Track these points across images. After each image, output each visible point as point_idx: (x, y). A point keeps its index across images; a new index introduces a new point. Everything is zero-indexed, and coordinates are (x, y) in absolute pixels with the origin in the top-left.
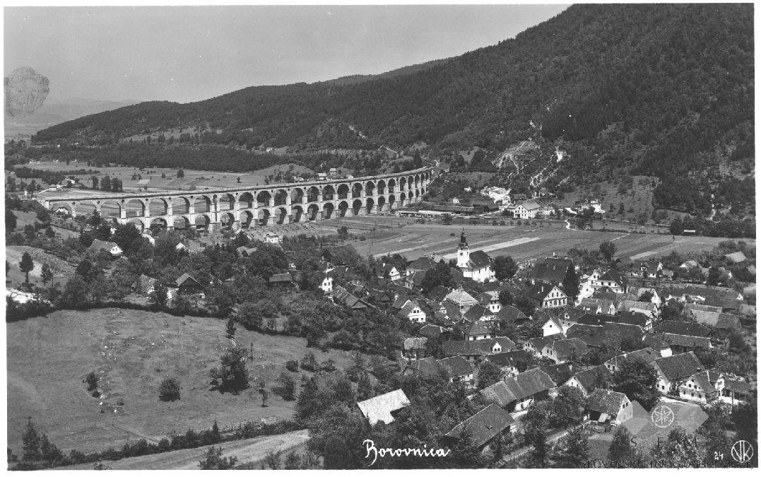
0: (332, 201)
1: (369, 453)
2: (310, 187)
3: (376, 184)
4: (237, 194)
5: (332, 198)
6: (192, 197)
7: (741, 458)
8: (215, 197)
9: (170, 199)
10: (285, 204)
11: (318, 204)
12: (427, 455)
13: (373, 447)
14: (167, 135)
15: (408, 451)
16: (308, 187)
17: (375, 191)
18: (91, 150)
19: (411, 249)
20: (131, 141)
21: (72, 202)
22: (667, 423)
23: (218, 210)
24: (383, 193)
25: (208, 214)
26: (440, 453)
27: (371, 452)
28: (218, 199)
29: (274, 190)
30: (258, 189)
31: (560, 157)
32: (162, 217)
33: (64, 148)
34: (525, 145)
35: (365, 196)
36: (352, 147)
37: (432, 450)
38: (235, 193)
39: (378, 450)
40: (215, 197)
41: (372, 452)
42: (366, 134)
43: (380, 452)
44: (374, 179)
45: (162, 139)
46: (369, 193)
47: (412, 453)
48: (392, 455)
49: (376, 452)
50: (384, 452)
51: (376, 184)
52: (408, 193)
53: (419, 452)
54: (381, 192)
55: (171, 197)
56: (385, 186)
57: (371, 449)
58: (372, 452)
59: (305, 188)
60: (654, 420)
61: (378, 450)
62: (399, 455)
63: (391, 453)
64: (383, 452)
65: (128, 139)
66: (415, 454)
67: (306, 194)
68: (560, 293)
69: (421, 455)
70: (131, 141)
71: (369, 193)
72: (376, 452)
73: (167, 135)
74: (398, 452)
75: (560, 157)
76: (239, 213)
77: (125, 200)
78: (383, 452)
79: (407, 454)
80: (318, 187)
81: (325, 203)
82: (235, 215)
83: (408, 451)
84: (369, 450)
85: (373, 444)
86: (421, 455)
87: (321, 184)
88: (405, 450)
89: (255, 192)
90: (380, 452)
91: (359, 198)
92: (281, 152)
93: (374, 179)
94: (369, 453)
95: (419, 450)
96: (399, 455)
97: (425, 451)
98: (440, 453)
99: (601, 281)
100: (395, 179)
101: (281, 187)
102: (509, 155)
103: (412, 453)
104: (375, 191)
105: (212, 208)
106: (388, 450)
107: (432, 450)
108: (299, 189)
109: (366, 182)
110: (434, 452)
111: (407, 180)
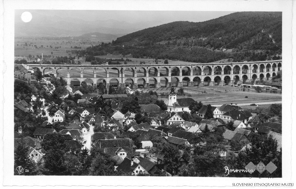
0: (189, 77)
1: (226, 171)
3: (232, 68)
4: (170, 67)
5: (230, 74)
6: (108, 68)
7: (19, 172)
8: (122, 69)
9: (108, 68)
11: (230, 76)
12: (247, 172)
13: (228, 169)
15: (240, 170)
16: (215, 66)
19: (204, 102)
22: (263, 170)
23: (124, 76)
24: (263, 71)
25: (167, 77)
26: (251, 171)
28: (123, 70)
29: (160, 67)
30: (149, 66)
32: (132, 78)
35: (272, 71)
37: (249, 170)
38: (135, 67)
39: (230, 170)
40: (122, 69)
43: (230, 171)
44: (231, 64)
46: (262, 70)
47: (242, 171)
51: (232, 68)
52: (272, 73)
55: (96, 67)
56: (264, 67)
57: (227, 170)
58: (227, 171)
59: (223, 66)
60: (258, 169)
62: (237, 172)
63: (234, 171)
66: (243, 171)
67: (192, 71)
68: (155, 123)
69: (245, 172)
71: (262, 70)
74: (237, 171)
77: (70, 67)
79: (240, 172)
80: (221, 66)
81: (184, 77)
82: (168, 79)
83: (240, 170)
86: (245, 172)
87: (192, 65)
88: (239, 170)
91: (219, 75)
93: (231, 64)
94: (226, 171)
95: (244, 170)
96: (237, 172)
98: (251, 171)
103: (242, 171)
104: (265, 70)
107: (249, 170)
108: (228, 66)
110: (249, 171)
111: (259, 67)
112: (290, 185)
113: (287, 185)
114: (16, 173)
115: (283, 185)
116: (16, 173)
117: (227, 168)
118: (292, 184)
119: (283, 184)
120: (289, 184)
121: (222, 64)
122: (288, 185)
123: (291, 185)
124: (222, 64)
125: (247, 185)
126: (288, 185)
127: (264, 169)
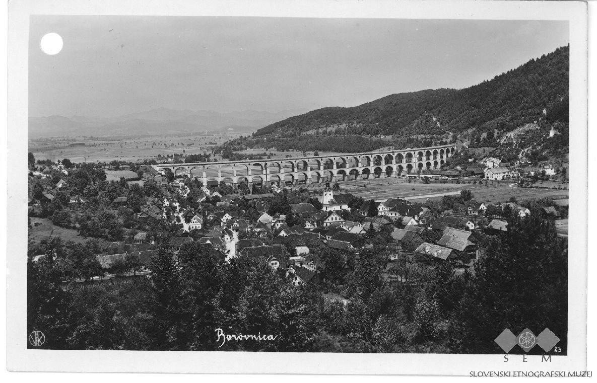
2: (386, 154)
6: (249, 164)
9: (249, 164)
10: (345, 167)
13: (222, 334)
14: (329, 130)
15: (247, 336)
17: (432, 157)
18: (283, 140)
20: (307, 134)
21: (233, 164)
22: (530, 344)
23: (268, 172)
26: (270, 338)
27: (220, 337)
29: (310, 159)
31: (552, 134)
33: (269, 141)
34: (528, 127)
36: (429, 133)
37: (265, 336)
39: (226, 336)
41: (222, 337)
42: (441, 124)
43: (227, 337)
45: (325, 133)
47: (250, 338)
48: (236, 339)
49: (224, 337)
50: (230, 337)
53: (255, 337)
54: (428, 159)
57: (221, 335)
58: (222, 337)
61: (226, 336)
63: (235, 338)
64: (229, 338)
65: (305, 133)
70: (307, 134)
72: (224, 337)
73: (329, 130)
75: (552, 134)
76: (283, 175)
77: (205, 166)
78: (229, 338)
80: (381, 155)
83: (247, 336)
84: (219, 336)
85: (222, 331)
86: (257, 339)
89: (295, 161)
90: (227, 337)
92: (389, 137)
96: (241, 339)
97: (259, 336)
98: (270, 338)
99: (390, 212)
100: (412, 153)
101: (367, 154)
102: (511, 134)
104: (432, 157)
105: (264, 172)
106: (233, 336)
107: (265, 336)
109: (426, 151)
110: (266, 337)
114: (30, 346)
115: (546, 361)
116: (30, 346)
117: (220, 333)
121: (188, 165)
123: (585, 374)
124: (188, 165)
127: (533, 344)
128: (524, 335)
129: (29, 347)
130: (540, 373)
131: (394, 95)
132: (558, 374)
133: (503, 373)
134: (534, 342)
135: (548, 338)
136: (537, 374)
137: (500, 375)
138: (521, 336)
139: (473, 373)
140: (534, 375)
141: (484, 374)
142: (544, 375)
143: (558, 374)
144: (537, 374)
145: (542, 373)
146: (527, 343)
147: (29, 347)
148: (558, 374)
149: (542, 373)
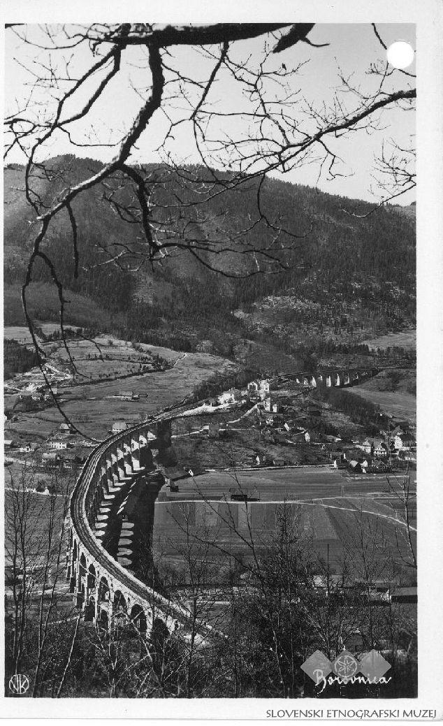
50: (333, 681)
53: (364, 681)
60: (338, 670)
86: (365, 683)
112: (427, 714)
113: (417, 714)
114: (9, 693)
115: (408, 716)
116: (9, 693)
118: (433, 712)
119: (408, 713)
120: (423, 713)
122: (422, 715)
125: (306, 716)
126: (422, 715)
128: (342, 660)
129: (7, 695)
130: (363, 712)
131: (220, 25)
132: (389, 713)
133: (312, 713)
134: (356, 669)
135: (374, 666)
136: (360, 714)
137: (309, 715)
138: (338, 661)
139: (271, 713)
140: (355, 714)
141: (286, 714)
142: (370, 714)
143: (389, 713)
144: (360, 714)
145: (367, 712)
146: (346, 671)
147: (7, 695)
148: (313, 713)
149: (367, 712)
